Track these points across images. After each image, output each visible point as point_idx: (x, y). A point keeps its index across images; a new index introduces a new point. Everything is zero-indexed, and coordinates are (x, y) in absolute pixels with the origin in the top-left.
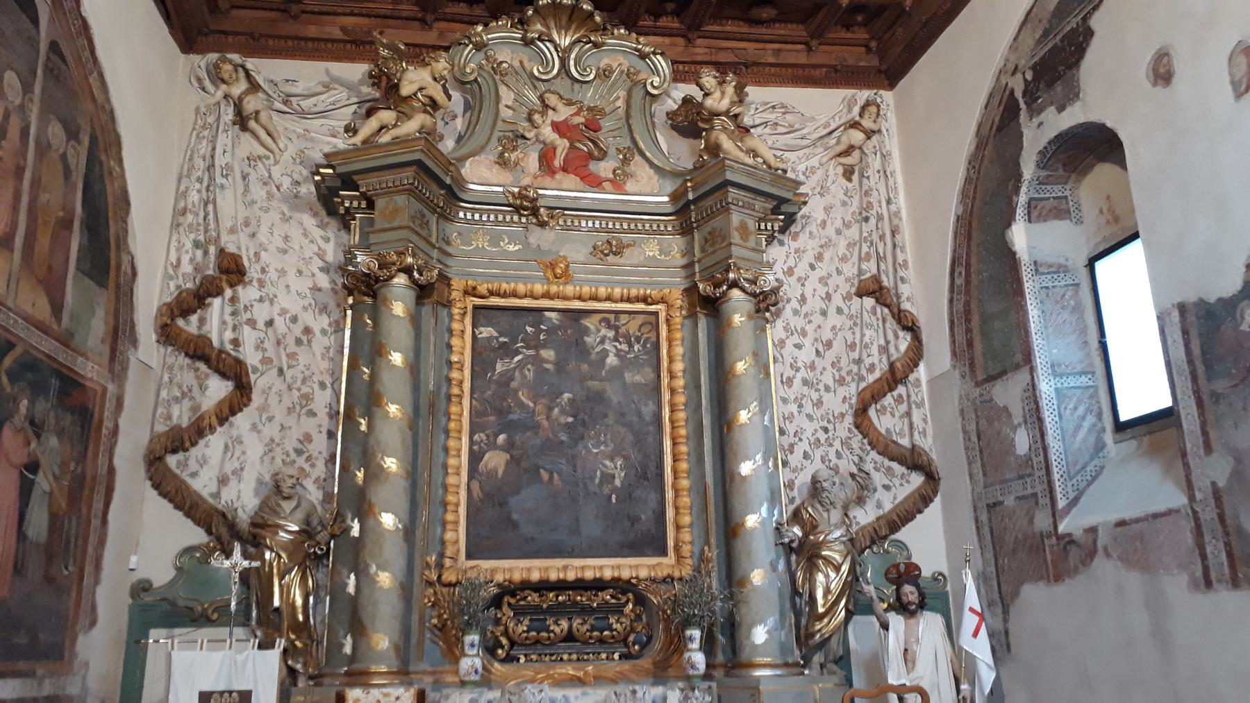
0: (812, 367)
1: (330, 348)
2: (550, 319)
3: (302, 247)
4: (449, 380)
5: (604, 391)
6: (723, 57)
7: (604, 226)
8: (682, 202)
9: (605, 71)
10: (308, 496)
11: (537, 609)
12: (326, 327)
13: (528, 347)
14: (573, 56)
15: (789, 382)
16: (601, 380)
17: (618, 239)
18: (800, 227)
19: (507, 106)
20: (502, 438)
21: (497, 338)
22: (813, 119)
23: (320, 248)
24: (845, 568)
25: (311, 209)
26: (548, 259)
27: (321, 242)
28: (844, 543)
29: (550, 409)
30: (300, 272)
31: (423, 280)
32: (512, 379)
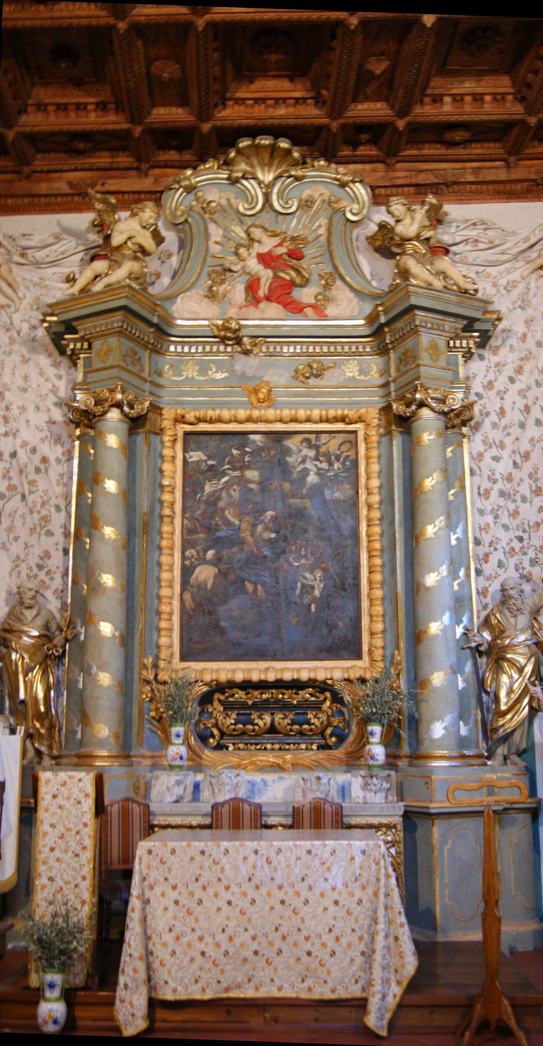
0: (509, 478)
1: (63, 475)
2: (254, 442)
3: (39, 386)
4: (161, 502)
5: (305, 508)
6: (421, 179)
7: (304, 350)
8: (376, 325)
9: (307, 201)
10: (49, 606)
11: (243, 705)
12: (60, 457)
13: (234, 469)
14: (275, 190)
15: (486, 494)
16: (302, 498)
17: (319, 362)
18: (500, 341)
19: (216, 243)
20: (210, 554)
21: (205, 461)
22: (514, 233)
23: (53, 386)
24: (529, 669)
25: (46, 351)
26: (251, 385)
27: (55, 380)
28: (529, 646)
29: (254, 526)
30: (38, 408)
31: (133, 413)
32: (219, 499)
